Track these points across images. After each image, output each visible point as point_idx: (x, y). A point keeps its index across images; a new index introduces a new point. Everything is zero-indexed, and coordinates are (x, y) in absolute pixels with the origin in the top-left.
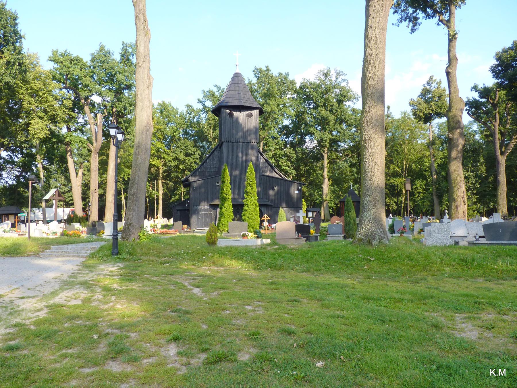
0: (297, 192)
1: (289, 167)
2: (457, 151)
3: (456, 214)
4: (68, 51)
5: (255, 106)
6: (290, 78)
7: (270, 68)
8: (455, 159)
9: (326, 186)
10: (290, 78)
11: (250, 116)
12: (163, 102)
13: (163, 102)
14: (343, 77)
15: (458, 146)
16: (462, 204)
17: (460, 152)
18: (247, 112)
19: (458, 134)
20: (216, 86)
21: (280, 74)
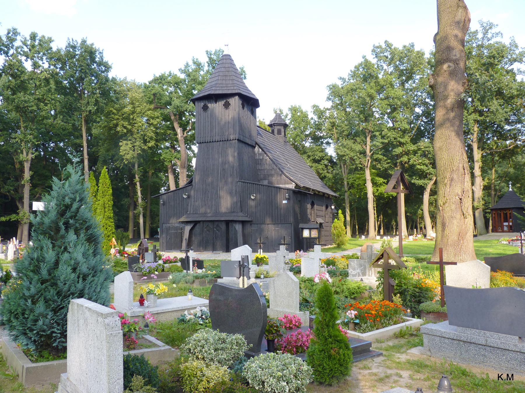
0: (285, 202)
1: (427, 166)
2: (445, 107)
3: (442, 237)
4: (172, 72)
5: (229, 92)
6: (417, 48)
7: (390, 41)
8: (442, 125)
9: (478, 187)
10: (417, 48)
11: (227, 105)
12: (292, 106)
13: (292, 106)
14: (494, 30)
15: (446, 98)
16: (458, 215)
17: (452, 109)
18: (223, 102)
19: (446, 75)
20: (341, 78)
21: (405, 47)
